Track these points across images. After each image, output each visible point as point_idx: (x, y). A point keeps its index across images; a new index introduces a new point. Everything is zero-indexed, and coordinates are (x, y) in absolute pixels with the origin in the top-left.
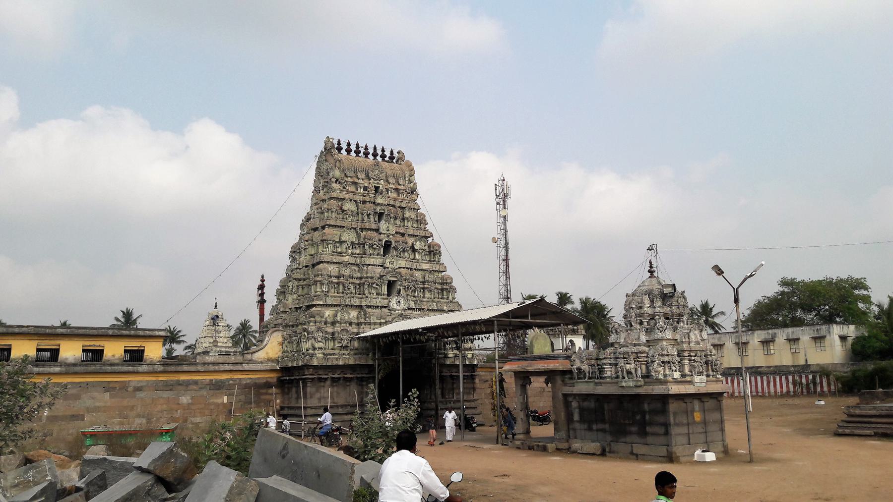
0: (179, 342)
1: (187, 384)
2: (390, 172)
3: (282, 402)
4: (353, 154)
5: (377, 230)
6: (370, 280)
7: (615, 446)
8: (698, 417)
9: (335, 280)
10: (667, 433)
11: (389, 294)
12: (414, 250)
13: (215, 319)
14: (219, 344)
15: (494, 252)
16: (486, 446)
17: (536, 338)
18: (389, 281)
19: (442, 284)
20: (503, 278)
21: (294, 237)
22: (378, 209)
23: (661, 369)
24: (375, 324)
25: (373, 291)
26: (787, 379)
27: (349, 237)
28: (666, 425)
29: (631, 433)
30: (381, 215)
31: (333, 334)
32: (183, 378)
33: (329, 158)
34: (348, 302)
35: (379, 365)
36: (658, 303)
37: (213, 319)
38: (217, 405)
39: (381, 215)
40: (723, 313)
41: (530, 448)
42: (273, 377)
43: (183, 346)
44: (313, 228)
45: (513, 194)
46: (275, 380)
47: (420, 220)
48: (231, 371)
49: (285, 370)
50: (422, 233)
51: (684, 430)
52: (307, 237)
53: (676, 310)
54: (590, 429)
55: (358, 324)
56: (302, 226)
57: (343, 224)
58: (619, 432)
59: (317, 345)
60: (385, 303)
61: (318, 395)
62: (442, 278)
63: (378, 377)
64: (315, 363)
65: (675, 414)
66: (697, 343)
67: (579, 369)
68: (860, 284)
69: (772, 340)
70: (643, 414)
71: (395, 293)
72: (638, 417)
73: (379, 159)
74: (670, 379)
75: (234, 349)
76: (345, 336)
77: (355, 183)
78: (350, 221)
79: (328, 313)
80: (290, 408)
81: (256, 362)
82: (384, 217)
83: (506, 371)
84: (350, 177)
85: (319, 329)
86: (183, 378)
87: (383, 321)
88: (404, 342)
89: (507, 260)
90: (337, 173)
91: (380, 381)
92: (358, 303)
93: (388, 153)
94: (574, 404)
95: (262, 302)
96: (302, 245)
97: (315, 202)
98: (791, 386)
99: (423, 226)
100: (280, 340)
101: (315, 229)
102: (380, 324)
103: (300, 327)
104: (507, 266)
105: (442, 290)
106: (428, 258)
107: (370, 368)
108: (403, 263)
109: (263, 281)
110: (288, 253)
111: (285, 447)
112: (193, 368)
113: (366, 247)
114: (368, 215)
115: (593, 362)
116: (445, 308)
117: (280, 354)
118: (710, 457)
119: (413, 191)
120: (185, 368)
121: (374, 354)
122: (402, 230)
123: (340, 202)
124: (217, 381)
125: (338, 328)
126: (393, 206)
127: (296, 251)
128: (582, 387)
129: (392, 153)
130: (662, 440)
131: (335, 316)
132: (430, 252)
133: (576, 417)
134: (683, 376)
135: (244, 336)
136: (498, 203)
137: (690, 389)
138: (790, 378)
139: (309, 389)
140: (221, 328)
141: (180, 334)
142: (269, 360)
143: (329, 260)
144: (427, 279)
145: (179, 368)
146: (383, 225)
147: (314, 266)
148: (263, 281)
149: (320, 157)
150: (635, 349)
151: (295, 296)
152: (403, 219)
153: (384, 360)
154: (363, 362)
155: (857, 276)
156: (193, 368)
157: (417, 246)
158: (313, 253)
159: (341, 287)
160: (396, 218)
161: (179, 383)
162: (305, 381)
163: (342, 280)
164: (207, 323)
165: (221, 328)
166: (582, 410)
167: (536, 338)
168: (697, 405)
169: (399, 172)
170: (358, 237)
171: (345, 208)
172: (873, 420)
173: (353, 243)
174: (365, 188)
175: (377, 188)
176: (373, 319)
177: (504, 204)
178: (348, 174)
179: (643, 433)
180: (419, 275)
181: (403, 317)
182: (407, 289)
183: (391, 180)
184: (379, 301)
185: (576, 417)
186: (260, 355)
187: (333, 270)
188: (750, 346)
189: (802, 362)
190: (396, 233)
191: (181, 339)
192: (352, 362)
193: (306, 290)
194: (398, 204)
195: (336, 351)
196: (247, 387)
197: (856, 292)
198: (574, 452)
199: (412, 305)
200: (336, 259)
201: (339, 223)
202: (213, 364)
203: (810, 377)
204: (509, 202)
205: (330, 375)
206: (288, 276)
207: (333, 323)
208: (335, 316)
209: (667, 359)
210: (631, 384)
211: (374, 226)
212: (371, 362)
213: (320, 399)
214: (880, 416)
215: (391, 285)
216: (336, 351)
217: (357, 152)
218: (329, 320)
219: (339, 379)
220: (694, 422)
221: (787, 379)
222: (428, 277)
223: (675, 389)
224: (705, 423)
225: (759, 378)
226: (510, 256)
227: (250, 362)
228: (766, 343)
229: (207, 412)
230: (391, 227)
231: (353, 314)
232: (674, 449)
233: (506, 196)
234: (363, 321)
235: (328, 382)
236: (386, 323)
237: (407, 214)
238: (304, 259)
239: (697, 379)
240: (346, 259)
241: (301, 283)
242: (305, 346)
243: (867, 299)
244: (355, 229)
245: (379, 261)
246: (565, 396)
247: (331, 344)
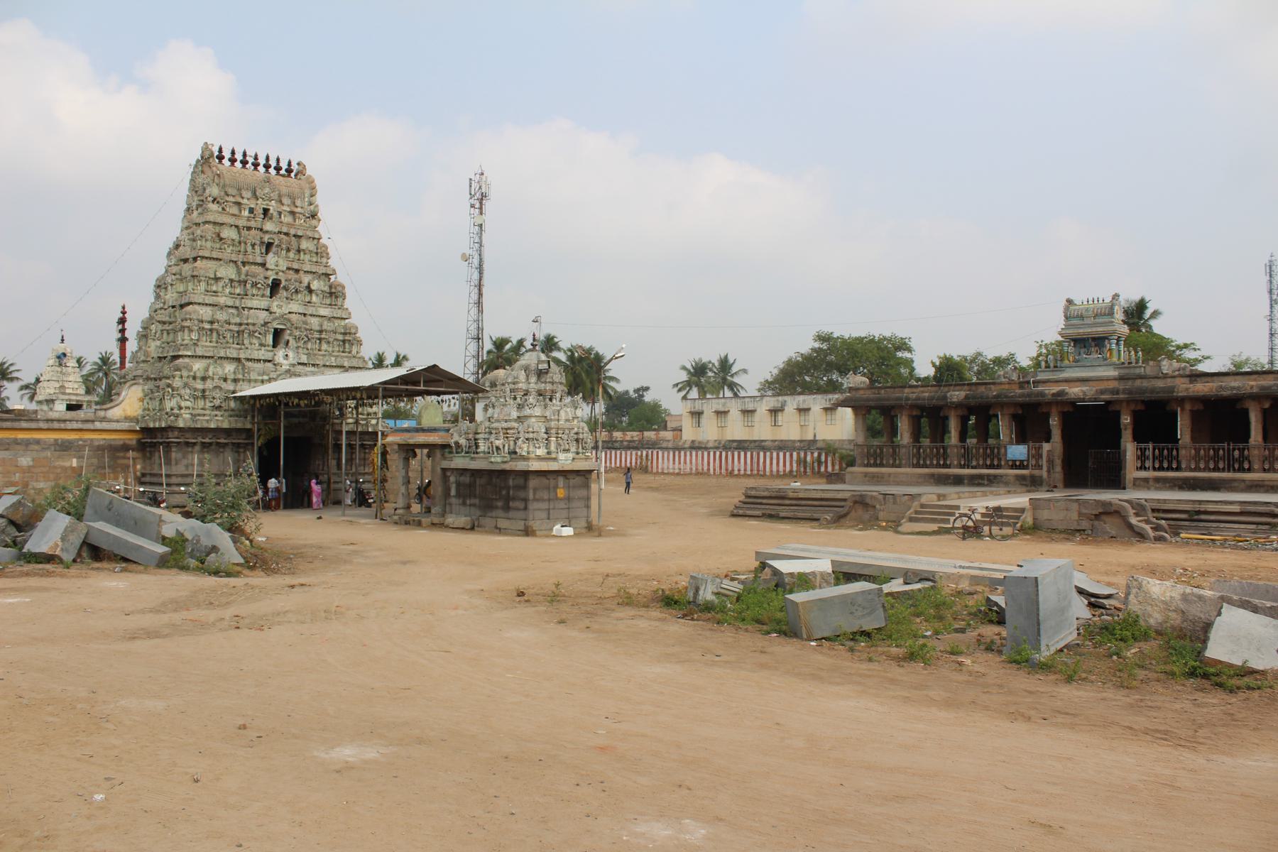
0: (12, 379)
1: (27, 443)
2: (284, 190)
3: (143, 468)
4: (238, 164)
5: (263, 265)
6: (251, 328)
7: (487, 521)
8: (561, 493)
9: (207, 326)
10: (526, 508)
11: (274, 346)
12: (311, 291)
13: (61, 357)
14: (68, 391)
15: (466, 273)
16: (363, 521)
17: (426, 407)
18: (276, 330)
19: (345, 334)
20: (474, 311)
21: (159, 266)
22: (266, 238)
23: (525, 446)
24: (256, 381)
25: (255, 341)
26: (791, 456)
27: (228, 272)
28: (526, 500)
29: (497, 508)
30: (269, 246)
31: (204, 391)
32: (21, 436)
33: (206, 169)
34: (222, 354)
35: (259, 430)
36: (533, 379)
37: (59, 357)
38: (65, 469)
39: (269, 246)
40: (745, 371)
41: (407, 523)
42: (132, 439)
43: (17, 385)
44: (183, 257)
45: (493, 194)
46: (134, 442)
47: (321, 253)
48: (81, 430)
49: (146, 431)
50: (322, 270)
51: (544, 505)
52: (175, 269)
53: (549, 387)
54: (464, 504)
55: (235, 381)
56: (169, 254)
57: (220, 255)
58: (487, 507)
59: (183, 404)
60: (269, 356)
61: (185, 462)
62: (345, 327)
63: (258, 443)
64: (181, 425)
65: (535, 490)
66: (567, 420)
67: (457, 443)
68: (903, 345)
69: (782, 410)
70: (508, 488)
71: (282, 345)
72: (504, 492)
73: (272, 171)
74: (532, 455)
75: (88, 398)
76: (217, 394)
77: (239, 204)
78: (228, 253)
79: (198, 366)
80: (151, 475)
81: (110, 421)
82: (274, 249)
83: (391, 444)
84: (230, 196)
85: (186, 385)
86: (21, 436)
87: (266, 377)
88: (287, 405)
89: (480, 286)
90: (214, 191)
91: (260, 448)
92: (235, 355)
93: (284, 165)
94: (452, 479)
95: (123, 340)
96: (169, 280)
97: (186, 224)
98: (795, 465)
99: (324, 260)
100: (141, 395)
101: (186, 261)
102: (263, 382)
103: (164, 381)
104: (480, 294)
105: (344, 341)
106: (328, 301)
107: (248, 433)
108: (294, 307)
109: (124, 313)
110: (152, 288)
111: (111, 503)
112: (33, 425)
113: (248, 286)
114: (253, 245)
115: (471, 436)
116: (346, 364)
117: (140, 412)
118: (568, 531)
119: (314, 216)
120: (24, 425)
121: (253, 417)
122: (295, 266)
123: (217, 229)
124: (64, 441)
125: (209, 384)
126: (287, 234)
127: (160, 286)
128: (459, 462)
129: (289, 164)
130: (521, 514)
131: (207, 370)
132: (331, 294)
133: (453, 492)
134: (549, 453)
135: (106, 374)
136: (472, 206)
137: (553, 466)
138: (795, 454)
139: (173, 455)
140: (70, 370)
141: (12, 369)
142: (127, 419)
143: (201, 301)
144: (325, 327)
145: (16, 425)
146: (271, 259)
147: (182, 306)
148: (124, 313)
149: (196, 166)
150: (505, 425)
151: (158, 343)
152: (299, 251)
153: (266, 424)
154: (239, 425)
155: (901, 334)
156: (33, 425)
157: (315, 286)
158: (181, 289)
159: (215, 334)
160: (288, 250)
161: (16, 442)
162: (168, 445)
163: (215, 326)
164: (51, 362)
165: (70, 370)
166: (458, 484)
167: (426, 407)
168: (561, 481)
169: (297, 191)
170: (239, 273)
171: (223, 235)
172: (1212, 517)
173: (231, 281)
174: (251, 211)
175: (266, 211)
176: (253, 376)
177: (481, 208)
178: (230, 191)
179: (507, 508)
180: (314, 322)
181: (290, 373)
182: (298, 339)
183: (286, 201)
184: (263, 354)
185: (453, 492)
186: (116, 412)
187: (206, 313)
188: (757, 415)
189: (811, 437)
190: (289, 269)
191: (14, 375)
192: (226, 425)
193: (171, 335)
194: (292, 232)
195: (207, 412)
196: (100, 449)
197: (899, 354)
198: (447, 527)
199: (304, 359)
200: (209, 300)
201: (215, 255)
202: (59, 421)
203: (816, 455)
204: (488, 205)
205: (200, 440)
206: (151, 317)
207: (204, 379)
208: (207, 370)
209: (531, 436)
210: (499, 460)
211: (259, 260)
212: (249, 426)
213: (187, 466)
214: (770, 498)
215: (277, 334)
216: (207, 412)
217: (244, 163)
218: (198, 375)
219: (211, 444)
220: (557, 499)
221: (791, 456)
222: (327, 325)
223: (535, 466)
224: (568, 499)
225: (762, 454)
226: (485, 281)
227: (103, 419)
228: (774, 412)
229: (52, 476)
230: (281, 262)
231: (229, 368)
232: (531, 523)
233: (483, 197)
234: (240, 376)
235: (197, 448)
236: (270, 380)
237: (305, 245)
238: (171, 297)
239: (562, 456)
240: (222, 300)
241: (166, 327)
242: (170, 404)
243: (909, 363)
244: (235, 262)
245: (264, 303)
246: (444, 470)
247: (201, 403)
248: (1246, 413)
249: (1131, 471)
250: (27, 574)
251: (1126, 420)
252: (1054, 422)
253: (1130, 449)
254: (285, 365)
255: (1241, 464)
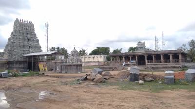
231: (22, 52)
243: (109, 50)
248: (169, 56)
249: (147, 63)
250: (24, 75)
251: (146, 57)
252: (137, 57)
253: (146, 61)
254: (31, 51)
255: (160, 62)
